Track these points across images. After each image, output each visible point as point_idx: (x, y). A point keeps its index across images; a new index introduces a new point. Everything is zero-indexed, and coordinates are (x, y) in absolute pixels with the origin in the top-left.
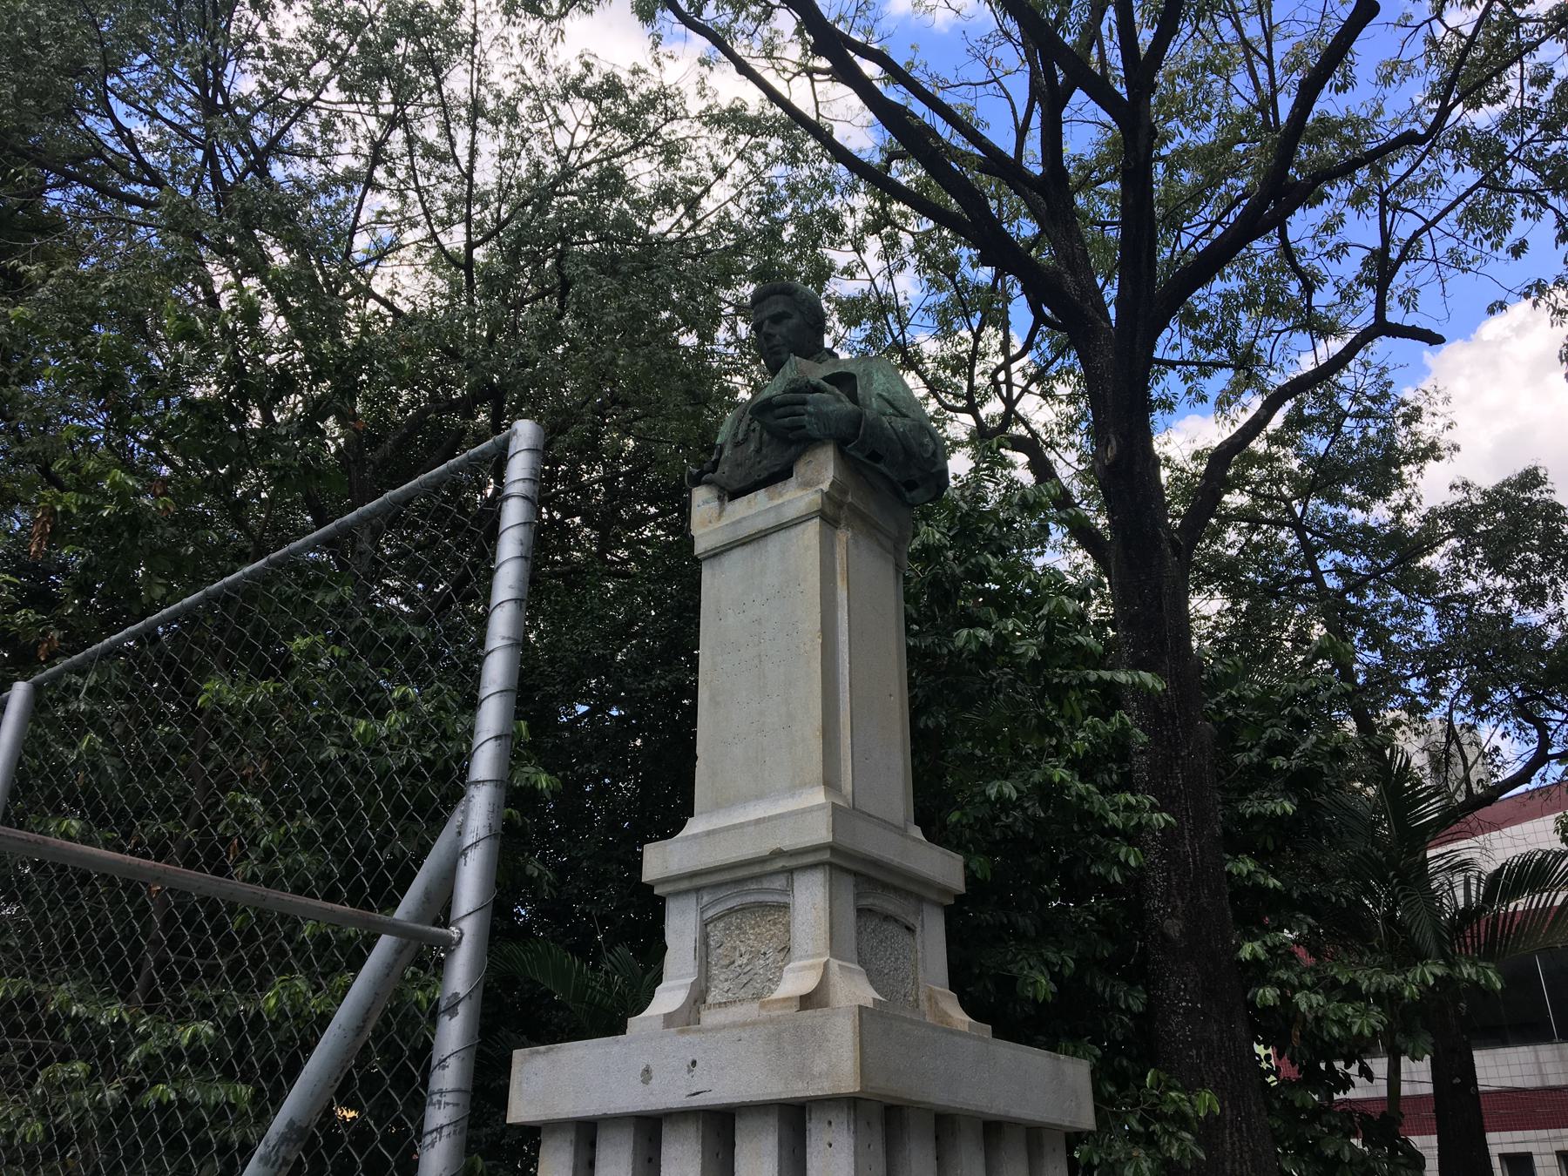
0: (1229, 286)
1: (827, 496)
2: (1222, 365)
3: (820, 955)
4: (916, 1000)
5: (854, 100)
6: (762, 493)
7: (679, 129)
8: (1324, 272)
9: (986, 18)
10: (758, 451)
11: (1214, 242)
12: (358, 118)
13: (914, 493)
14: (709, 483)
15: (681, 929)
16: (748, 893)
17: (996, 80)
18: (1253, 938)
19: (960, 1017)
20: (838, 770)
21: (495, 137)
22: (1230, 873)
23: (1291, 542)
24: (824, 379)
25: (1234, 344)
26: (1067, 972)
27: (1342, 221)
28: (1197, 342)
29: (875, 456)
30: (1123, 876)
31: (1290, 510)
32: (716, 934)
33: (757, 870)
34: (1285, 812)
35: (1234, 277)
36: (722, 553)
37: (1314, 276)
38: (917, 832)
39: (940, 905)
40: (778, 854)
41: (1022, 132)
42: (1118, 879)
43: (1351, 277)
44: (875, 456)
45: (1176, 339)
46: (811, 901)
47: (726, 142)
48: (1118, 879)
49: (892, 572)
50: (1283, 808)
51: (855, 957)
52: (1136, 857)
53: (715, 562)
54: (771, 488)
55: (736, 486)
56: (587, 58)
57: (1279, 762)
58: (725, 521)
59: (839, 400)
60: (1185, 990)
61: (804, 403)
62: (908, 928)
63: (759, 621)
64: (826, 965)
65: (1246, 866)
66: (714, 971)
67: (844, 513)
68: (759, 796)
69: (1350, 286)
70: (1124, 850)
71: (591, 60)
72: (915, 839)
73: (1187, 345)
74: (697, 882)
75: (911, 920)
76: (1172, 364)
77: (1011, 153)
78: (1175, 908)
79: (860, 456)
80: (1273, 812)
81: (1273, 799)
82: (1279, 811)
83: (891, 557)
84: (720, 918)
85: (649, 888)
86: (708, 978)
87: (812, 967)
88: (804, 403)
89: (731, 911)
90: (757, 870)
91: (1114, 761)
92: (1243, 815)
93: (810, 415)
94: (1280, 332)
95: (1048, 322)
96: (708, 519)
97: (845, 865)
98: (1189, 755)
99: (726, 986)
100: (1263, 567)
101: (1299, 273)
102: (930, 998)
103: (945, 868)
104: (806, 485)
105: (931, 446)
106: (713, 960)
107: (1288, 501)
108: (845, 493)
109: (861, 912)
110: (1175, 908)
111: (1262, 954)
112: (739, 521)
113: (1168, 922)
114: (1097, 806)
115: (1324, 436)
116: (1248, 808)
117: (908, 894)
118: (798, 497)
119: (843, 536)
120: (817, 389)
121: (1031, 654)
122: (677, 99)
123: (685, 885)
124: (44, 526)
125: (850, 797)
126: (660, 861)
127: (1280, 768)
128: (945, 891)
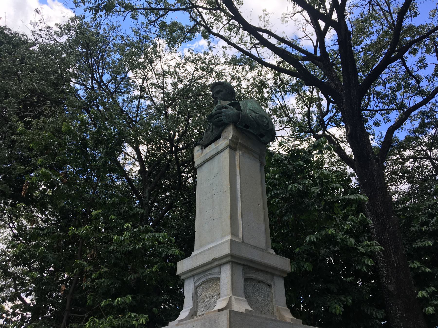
0: (391, 85)
1: (231, 141)
2: (393, 109)
3: (229, 295)
4: (273, 312)
5: (270, 51)
6: (213, 144)
7: (218, 68)
8: (422, 76)
9: (290, 7)
10: (212, 132)
11: (378, 64)
12: (135, 80)
13: (264, 138)
14: (199, 144)
15: (189, 291)
16: (208, 275)
17: (307, 35)
18: (422, 290)
19: (288, 316)
20: (238, 229)
21: (171, 78)
22: (411, 267)
23: (429, 165)
24: (228, 105)
25: (396, 102)
26: (349, 304)
27: (425, 59)
28: (384, 103)
29: (247, 127)
30: (367, 269)
31: (426, 154)
32: (200, 291)
33: (209, 266)
34: (429, 245)
35: (393, 82)
36: (202, 165)
37: (419, 78)
38: (272, 252)
39: (282, 277)
40: (215, 260)
41: (316, 48)
42: (365, 270)
43: (430, 75)
44: (247, 127)
45: (377, 104)
46: (226, 275)
47: (233, 69)
48: (365, 270)
49: (258, 164)
50: (428, 244)
51: (243, 295)
52: (371, 262)
53: (200, 168)
54: (216, 142)
55: (206, 143)
56: (191, 51)
57: (425, 228)
58: (203, 155)
59: (232, 110)
60: (398, 310)
61: (222, 112)
62: (269, 285)
63: (212, 184)
64: (230, 298)
65: (417, 264)
66: (199, 304)
67: (238, 146)
68: (213, 242)
69: (431, 77)
70: (367, 259)
71: (192, 52)
72: (270, 253)
73: (381, 105)
74: (193, 273)
75: (269, 282)
76: (377, 111)
77: (313, 53)
78: (391, 281)
79: (241, 127)
80: (425, 245)
81: (424, 241)
82: (427, 245)
83: (258, 160)
84: (200, 285)
85: (179, 276)
86: (197, 307)
87: (225, 299)
88: (222, 112)
89: (204, 282)
90: (209, 266)
91: (366, 233)
92: (415, 248)
93: (224, 116)
94: (411, 97)
95: (332, 102)
96: (199, 155)
97: (234, 260)
98: (390, 227)
99: (203, 309)
100: (421, 173)
101: (415, 77)
102: (277, 310)
103: (284, 264)
104: (225, 139)
105: (266, 122)
106: (199, 300)
107: (425, 151)
108: (238, 139)
109: (246, 280)
110: (391, 281)
111: (426, 295)
112: (206, 154)
113: (389, 286)
114: (349, 243)
115: (433, 128)
116: (417, 245)
117: (267, 273)
118: (222, 143)
119: (238, 153)
120: (226, 107)
121: (316, 191)
122: (218, 59)
123: (189, 274)
124: (26, 187)
125: (242, 239)
126: (183, 266)
127: (425, 230)
128: (283, 271)
